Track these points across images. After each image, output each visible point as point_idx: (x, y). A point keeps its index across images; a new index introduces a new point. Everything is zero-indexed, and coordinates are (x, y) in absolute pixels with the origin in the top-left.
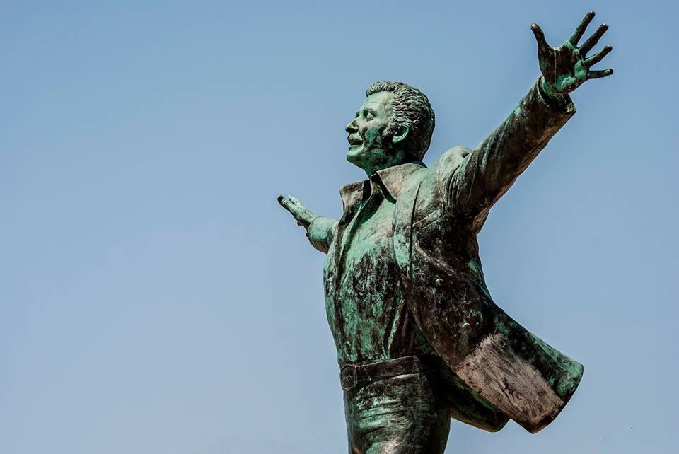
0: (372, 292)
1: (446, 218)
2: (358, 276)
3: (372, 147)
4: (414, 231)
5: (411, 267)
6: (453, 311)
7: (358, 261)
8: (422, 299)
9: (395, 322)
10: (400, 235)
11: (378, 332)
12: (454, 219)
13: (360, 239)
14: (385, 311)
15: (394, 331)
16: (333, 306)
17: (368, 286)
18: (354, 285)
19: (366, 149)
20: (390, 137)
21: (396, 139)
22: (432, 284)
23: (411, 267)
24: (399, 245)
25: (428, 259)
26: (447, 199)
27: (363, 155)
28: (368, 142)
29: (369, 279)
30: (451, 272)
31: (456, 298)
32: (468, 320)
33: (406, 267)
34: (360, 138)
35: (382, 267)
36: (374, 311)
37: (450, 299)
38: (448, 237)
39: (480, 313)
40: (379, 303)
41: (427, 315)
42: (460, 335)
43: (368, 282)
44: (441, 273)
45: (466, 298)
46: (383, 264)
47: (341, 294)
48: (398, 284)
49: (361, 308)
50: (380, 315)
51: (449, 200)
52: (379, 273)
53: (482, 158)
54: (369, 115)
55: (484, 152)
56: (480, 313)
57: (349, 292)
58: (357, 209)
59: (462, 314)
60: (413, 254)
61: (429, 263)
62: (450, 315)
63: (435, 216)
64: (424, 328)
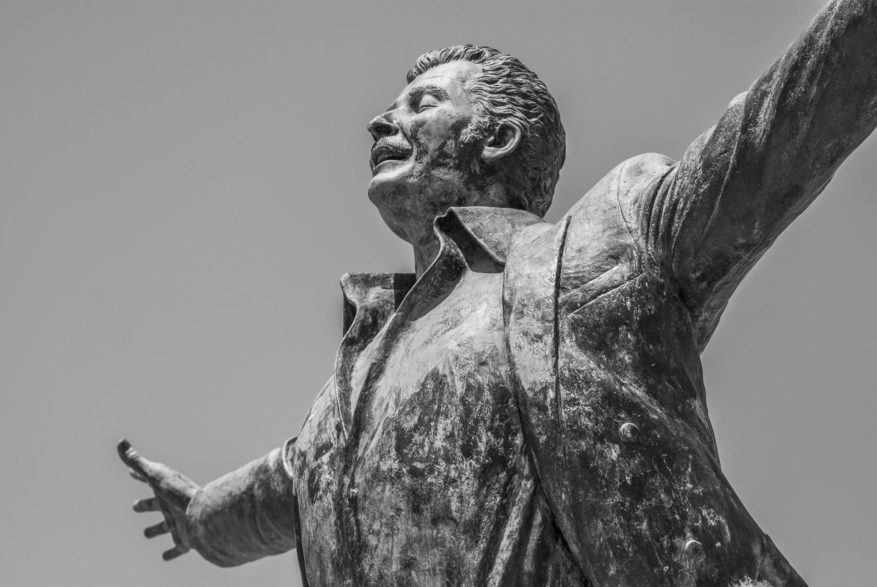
0: (449, 460)
1: (642, 282)
2: (410, 423)
3: (435, 163)
4: (563, 310)
5: (557, 392)
6: (660, 507)
7: (410, 391)
8: (585, 470)
9: (507, 533)
10: (525, 321)
11: (461, 559)
12: (661, 287)
13: (412, 349)
14: (481, 506)
15: (504, 554)
16: (333, 518)
17: (439, 443)
18: (399, 449)
19: (419, 167)
20: (475, 146)
21: (488, 152)
22: (609, 435)
23: (557, 392)
24: (523, 342)
25: (600, 374)
26: (647, 239)
27: (411, 180)
28: (426, 152)
29: (443, 426)
30: (656, 412)
31: (667, 475)
32: (695, 532)
33: (544, 390)
34: (406, 144)
35: (478, 399)
36: (454, 505)
37: (654, 473)
38: (648, 327)
39: (723, 521)
40: (468, 486)
41: (595, 512)
42: (677, 567)
43: (441, 433)
44: (632, 408)
45: (691, 477)
46: (480, 390)
47: (359, 479)
48: (519, 440)
49: (417, 501)
50: (469, 514)
51: (652, 240)
52: (468, 411)
53: (757, 112)
54: (427, 99)
55: (765, 94)
56: (723, 521)
57: (384, 467)
58: (385, 318)
59: (684, 516)
60: (561, 363)
61: (602, 384)
62: (655, 514)
63: (618, 277)
64: (586, 547)
